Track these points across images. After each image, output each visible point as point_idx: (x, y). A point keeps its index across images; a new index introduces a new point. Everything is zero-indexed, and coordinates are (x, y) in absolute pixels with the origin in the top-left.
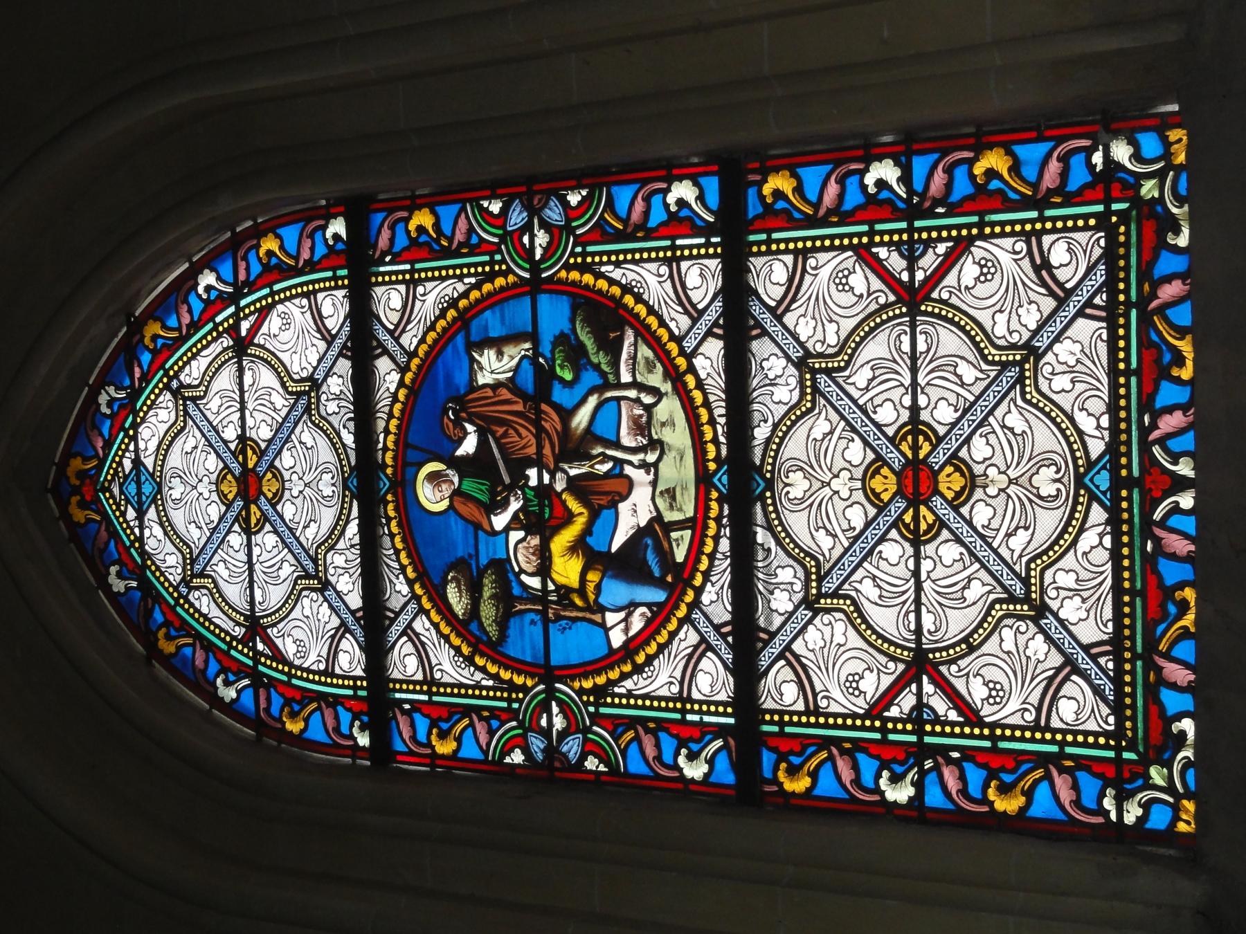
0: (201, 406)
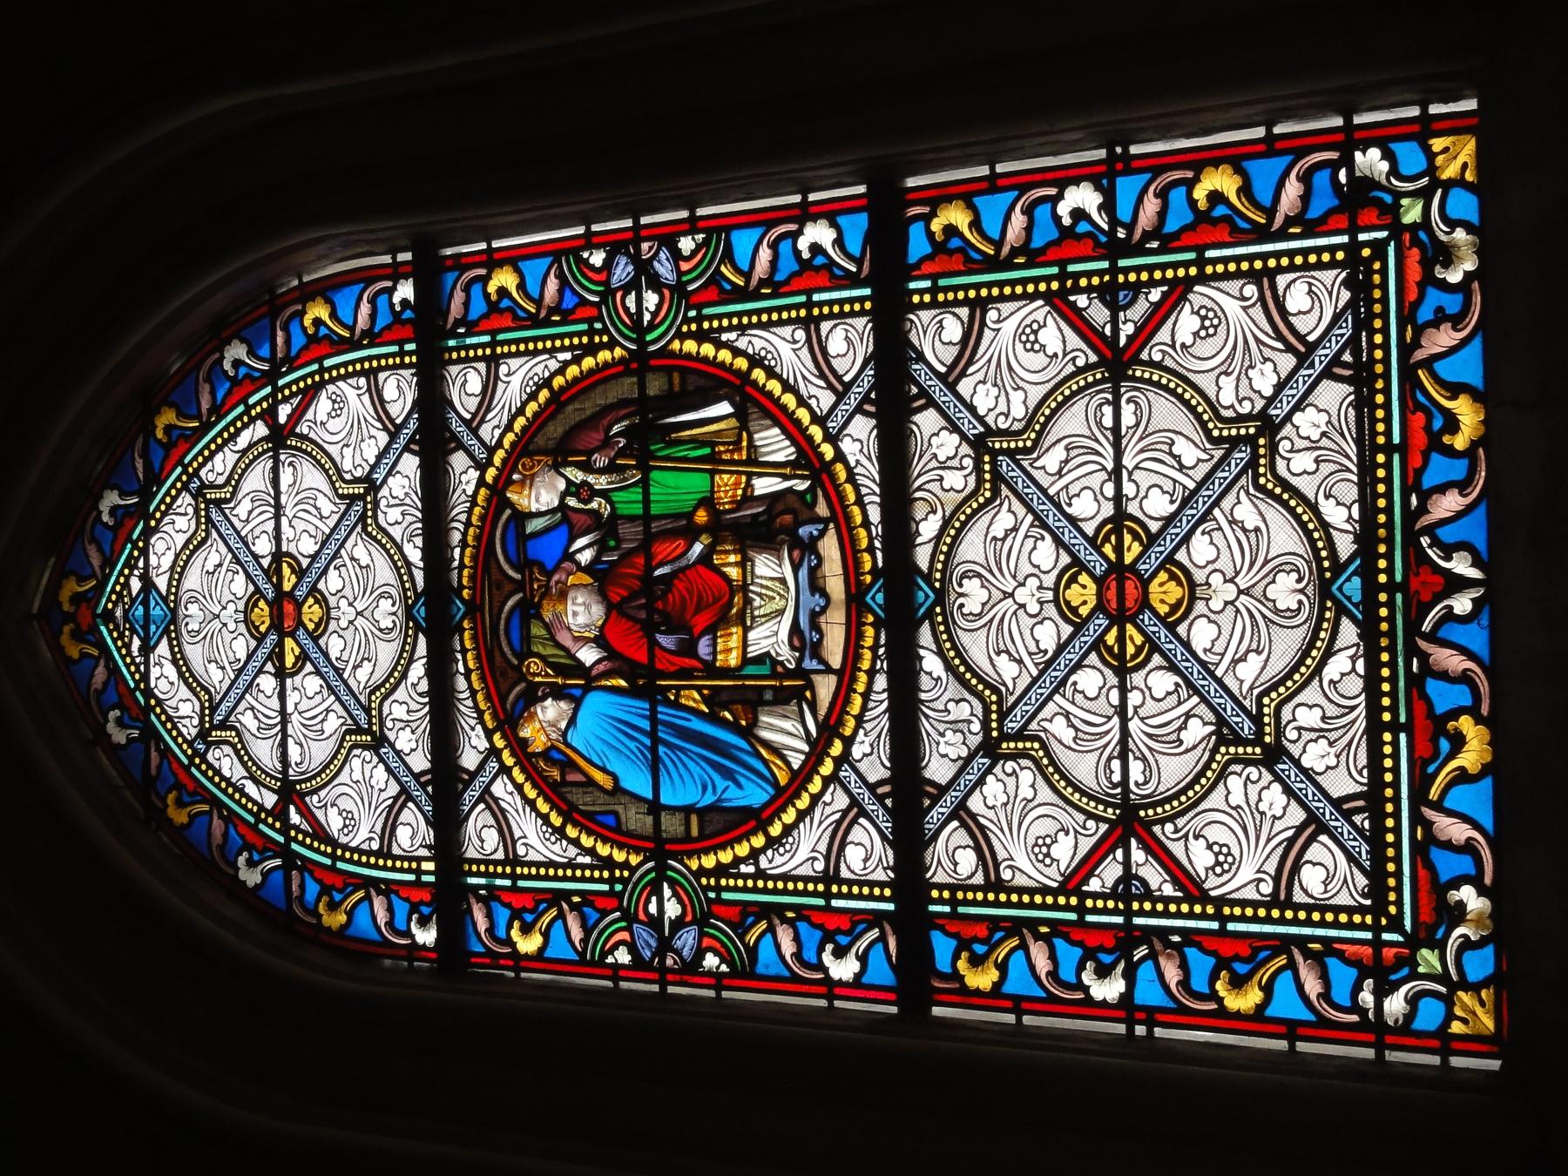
0: (227, 511)
